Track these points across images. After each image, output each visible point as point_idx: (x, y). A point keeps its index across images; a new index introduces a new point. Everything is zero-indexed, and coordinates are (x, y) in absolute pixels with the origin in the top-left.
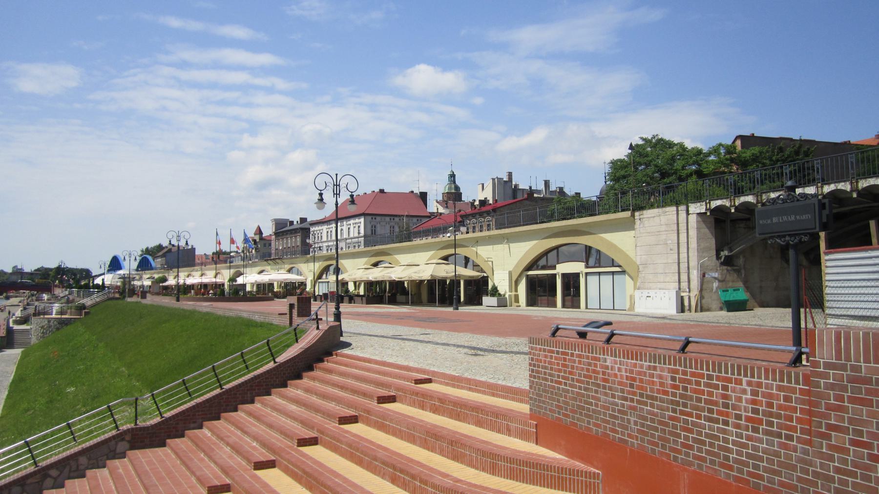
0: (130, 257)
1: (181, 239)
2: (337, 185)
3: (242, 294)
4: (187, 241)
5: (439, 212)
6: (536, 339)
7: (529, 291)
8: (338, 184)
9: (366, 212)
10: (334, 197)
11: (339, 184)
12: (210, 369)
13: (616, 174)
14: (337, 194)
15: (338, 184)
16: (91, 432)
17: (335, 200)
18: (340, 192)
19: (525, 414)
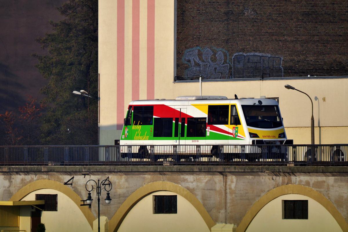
0: (99, 193)
1: (102, 191)
2: (99, 187)
3: (179, 123)
4: (108, 194)
5: (181, 111)
6: (251, 158)
7: (191, 117)
8: (99, 186)
9: (72, 179)
10: (97, 195)
11: (100, 186)
12: (43, 168)
13: (192, 180)
14: (99, 193)
15: (99, 186)
16: (72, 157)
17: (98, 197)
18: (100, 191)
19: (154, 98)
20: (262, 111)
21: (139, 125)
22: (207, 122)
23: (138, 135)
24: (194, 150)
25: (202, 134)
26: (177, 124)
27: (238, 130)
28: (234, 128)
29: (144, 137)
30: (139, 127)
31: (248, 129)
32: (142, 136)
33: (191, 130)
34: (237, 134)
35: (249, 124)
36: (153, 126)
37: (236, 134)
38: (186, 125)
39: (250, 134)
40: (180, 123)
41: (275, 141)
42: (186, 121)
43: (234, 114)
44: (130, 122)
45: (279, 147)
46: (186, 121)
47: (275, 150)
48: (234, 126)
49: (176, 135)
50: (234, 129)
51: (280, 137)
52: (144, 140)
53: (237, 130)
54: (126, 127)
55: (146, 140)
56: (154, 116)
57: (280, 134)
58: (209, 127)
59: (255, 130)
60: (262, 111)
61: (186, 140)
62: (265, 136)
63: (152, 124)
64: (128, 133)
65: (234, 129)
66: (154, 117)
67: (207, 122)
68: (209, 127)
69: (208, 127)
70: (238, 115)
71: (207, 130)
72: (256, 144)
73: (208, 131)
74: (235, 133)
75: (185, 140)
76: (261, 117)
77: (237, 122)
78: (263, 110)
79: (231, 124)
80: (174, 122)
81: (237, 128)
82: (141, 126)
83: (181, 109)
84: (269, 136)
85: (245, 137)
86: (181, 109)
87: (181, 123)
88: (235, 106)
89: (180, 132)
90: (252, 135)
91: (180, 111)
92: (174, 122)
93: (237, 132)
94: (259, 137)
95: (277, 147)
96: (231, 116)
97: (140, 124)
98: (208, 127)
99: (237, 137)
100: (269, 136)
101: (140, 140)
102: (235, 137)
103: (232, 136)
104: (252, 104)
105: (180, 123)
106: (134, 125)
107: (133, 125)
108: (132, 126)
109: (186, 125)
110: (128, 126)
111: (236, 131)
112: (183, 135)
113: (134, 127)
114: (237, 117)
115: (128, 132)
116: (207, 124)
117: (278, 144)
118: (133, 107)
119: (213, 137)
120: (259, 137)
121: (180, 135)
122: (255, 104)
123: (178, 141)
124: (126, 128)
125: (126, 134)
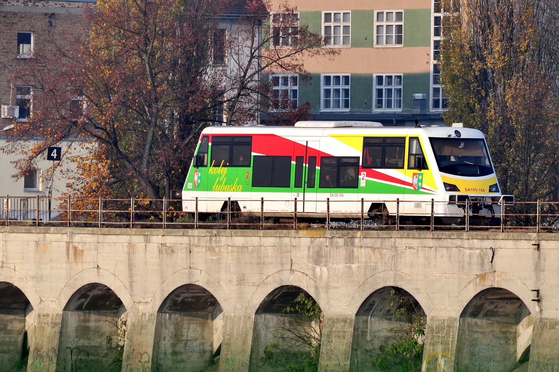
3: (304, 165)
5: (308, 146)
20: (460, 147)
21: (223, 166)
22: (361, 164)
23: (220, 183)
24: (45, 209)
25: (353, 185)
26: (299, 168)
27: (422, 177)
28: (414, 174)
29: (233, 186)
30: (222, 171)
31: (442, 177)
32: (229, 184)
33: (327, 177)
34: (422, 184)
35: (442, 169)
36: (250, 169)
37: (420, 184)
38: (318, 168)
39: (445, 184)
40: (306, 166)
41: (483, 197)
42: (318, 160)
43: (414, 152)
44: (203, 161)
45: (490, 208)
46: (318, 160)
47: (484, 212)
48: (416, 171)
49: (298, 185)
50: (415, 176)
51: (490, 191)
52: (234, 191)
53: (420, 177)
54: (196, 169)
55: (237, 191)
56: (254, 152)
57: (490, 187)
58: (365, 173)
59: (452, 179)
60: (460, 147)
61: (405, 195)
62: (469, 190)
63: (249, 166)
64: (200, 179)
65: (415, 176)
66: (253, 154)
67: (361, 164)
68: (365, 173)
69: (362, 173)
70: (422, 154)
71: (360, 177)
72: (458, 201)
73: (363, 179)
74: (418, 184)
75: (315, 194)
76: (455, 157)
77: (421, 164)
78: (462, 145)
79: (409, 168)
80: (293, 163)
81: (422, 174)
82: (226, 168)
83: (307, 142)
84: (475, 190)
85: (437, 190)
86: (307, 142)
87: (307, 165)
88: (417, 138)
89: (306, 180)
90: (451, 187)
91: (306, 145)
92: (293, 163)
93: (421, 181)
94: (459, 191)
95: (118, 208)
96: (410, 154)
97: (224, 166)
98: (362, 173)
99: (421, 190)
100: (475, 190)
101: (224, 191)
102: (416, 189)
103: (412, 188)
104: (446, 136)
105: (306, 166)
106: (213, 167)
107: (211, 166)
108: (209, 170)
109: (318, 168)
110: (200, 168)
111: (198, 176)
112: (311, 185)
113: (212, 170)
114: (421, 156)
115: (199, 178)
116: (360, 167)
117: (489, 202)
118: (210, 138)
119: (370, 189)
120: (459, 191)
121: (306, 185)
122: (450, 136)
123: (301, 194)
124: (196, 171)
125: (195, 181)
